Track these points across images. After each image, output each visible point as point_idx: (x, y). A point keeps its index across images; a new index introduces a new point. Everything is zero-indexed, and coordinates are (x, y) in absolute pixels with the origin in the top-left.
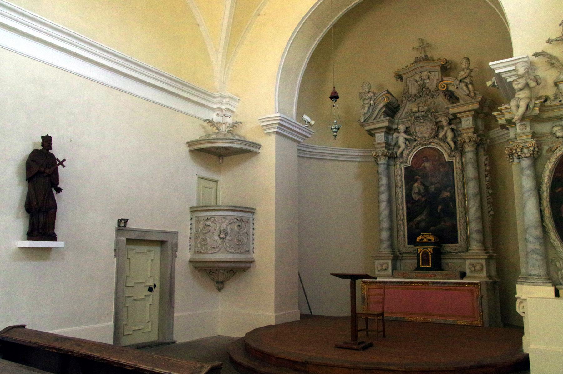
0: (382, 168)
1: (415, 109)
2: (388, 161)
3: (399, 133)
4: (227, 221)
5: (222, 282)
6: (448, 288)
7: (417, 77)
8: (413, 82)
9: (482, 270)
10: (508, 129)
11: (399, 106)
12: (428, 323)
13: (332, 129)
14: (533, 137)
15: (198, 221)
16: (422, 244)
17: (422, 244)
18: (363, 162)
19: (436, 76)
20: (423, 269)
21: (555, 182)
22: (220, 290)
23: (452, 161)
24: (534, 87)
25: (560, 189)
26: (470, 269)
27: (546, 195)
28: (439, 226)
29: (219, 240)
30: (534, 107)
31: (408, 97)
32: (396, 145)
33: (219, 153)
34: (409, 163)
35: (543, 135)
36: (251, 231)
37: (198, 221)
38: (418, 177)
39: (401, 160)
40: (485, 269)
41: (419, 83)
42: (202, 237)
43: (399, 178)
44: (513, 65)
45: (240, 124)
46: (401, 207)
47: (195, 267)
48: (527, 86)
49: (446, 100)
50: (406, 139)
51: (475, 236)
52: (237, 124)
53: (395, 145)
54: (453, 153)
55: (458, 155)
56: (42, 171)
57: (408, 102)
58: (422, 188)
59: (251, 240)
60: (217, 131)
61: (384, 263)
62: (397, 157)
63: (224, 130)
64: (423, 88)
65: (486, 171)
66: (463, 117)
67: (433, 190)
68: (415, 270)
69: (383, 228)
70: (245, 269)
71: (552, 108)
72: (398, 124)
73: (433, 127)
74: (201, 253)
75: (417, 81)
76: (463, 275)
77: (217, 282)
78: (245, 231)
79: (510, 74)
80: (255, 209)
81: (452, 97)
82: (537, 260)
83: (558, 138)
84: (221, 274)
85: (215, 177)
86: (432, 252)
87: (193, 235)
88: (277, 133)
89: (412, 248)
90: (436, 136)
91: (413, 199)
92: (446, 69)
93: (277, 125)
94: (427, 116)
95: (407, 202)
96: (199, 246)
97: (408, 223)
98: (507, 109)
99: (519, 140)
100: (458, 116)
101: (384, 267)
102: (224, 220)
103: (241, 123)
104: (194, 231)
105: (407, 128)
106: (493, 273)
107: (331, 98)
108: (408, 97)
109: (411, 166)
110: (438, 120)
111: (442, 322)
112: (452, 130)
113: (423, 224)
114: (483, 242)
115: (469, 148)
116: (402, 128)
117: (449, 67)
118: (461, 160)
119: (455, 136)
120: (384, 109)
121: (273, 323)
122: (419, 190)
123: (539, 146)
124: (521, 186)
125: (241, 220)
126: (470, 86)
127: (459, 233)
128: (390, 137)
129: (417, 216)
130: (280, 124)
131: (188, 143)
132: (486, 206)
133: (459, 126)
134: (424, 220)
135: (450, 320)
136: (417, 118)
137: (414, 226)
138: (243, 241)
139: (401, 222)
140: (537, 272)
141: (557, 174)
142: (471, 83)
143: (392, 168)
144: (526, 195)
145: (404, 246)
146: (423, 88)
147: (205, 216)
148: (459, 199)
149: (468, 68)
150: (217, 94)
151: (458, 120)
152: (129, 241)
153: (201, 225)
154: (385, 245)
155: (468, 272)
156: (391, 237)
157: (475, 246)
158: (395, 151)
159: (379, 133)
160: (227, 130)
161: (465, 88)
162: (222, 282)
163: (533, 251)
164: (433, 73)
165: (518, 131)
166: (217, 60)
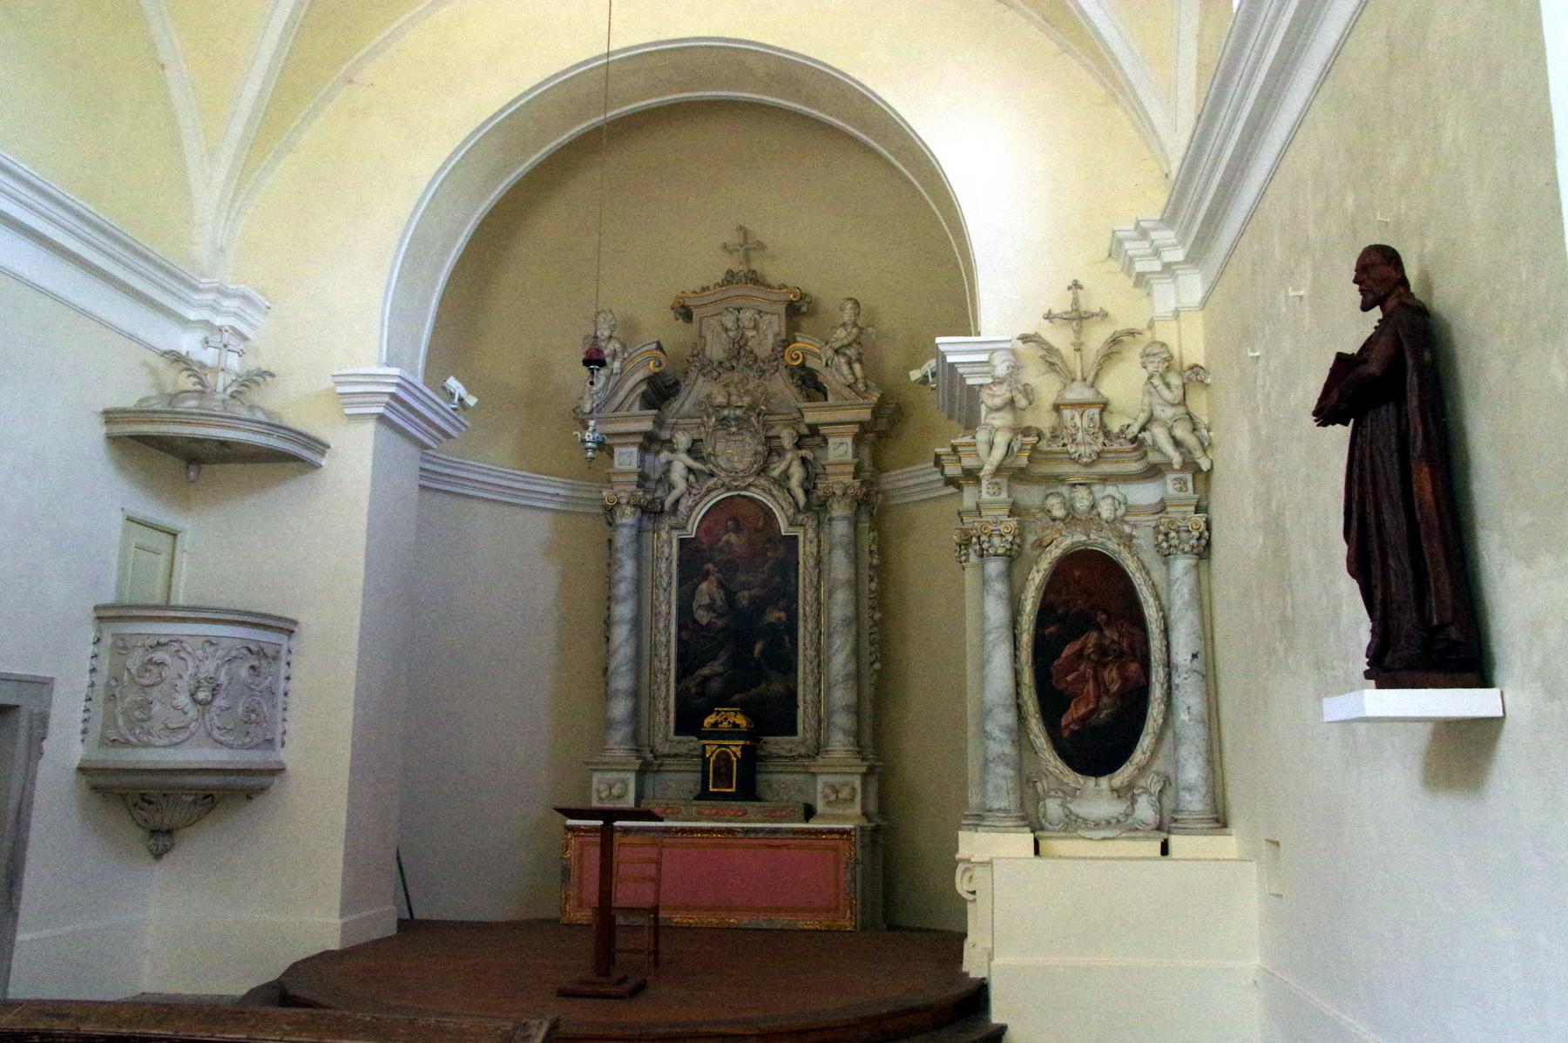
0: (624, 537)
1: (720, 399)
2: (640, 521)
3: (673, 451)
5: (169, 832)
6: (779, 842)
7: (729, 321)
9: (852, 800)
10: (959, 487)
11: (677, 383)
12: (730, 929)
13: (584, 441)
14: (1011, 514)
15: (125, 648)
16: (716, 733)
18: (558, 511)
19: (774, 325)
20: (715, 796)
21: (1045, 612)
22: (158, 856)
23: (796, 537)
24: (1024, 410)
25: (1052, 629)
27: (1026, 639)
30: (1020, 450)
31: (703, 367)
32: (665, 480)
33: (190, 453)
34: (691, 531)
35: (1027, 509)
36: (282, 683)
37: (122, 647)
38: (710, 566)
39: (673, 521)
40: (858, 798)
41: (731, 334)
42: (133, 696)
43: (663, 566)
44: (985, 351)
46: (663, 639)
47: (95, 788)
48: (1012, 402)
49: (795, 390)
50: (690, 470)
52: (253, 380)
53: (659, 481)
54: (800, 517)
55: (811, 524)
57: (701, 379)
58: (719, 595)
59: (280, 707)
60: (198, 387)
61: (617, 780)
62: (662, 511)
63: (220, 388)
64: (739, 348)
65: (871, 567)
66: (834, 435)
67: (745, 603)
68: (697, 798)
69: (617, 691)
70: (250, 794)
71: (1051, 456)
72: (674, 428)
73: (760, 448)
74: (127, 743)
75: (727, 330)
76: (809, 812)
78: (267, 683)
79: (976, 369)
80: (295, 623)
81: (810, 384)
82: (1005, 777)
83: (1054, 520)
84: (157, 808)
85: (168, 519)
87: (100, 688)
88: (381, 418)
89: (691, 743)
90: (763, 470)
91: (695, 621)
92: (798, 310)
93: (387, 399)
94: (747, 420)
95: (680, 628)
96: (120, 722)
97: (678, 681)
98: (969, 445)
100: (823, 430)
101: (615, 791)
102: (210, 650)
103: (272, 375)
104: (101, 679)
105: (694, 441)
106: (873, 807)
107: (586, 363)
108: (703, 367)
110: (770, 433)
112: (804, 460)
113: (715, 685)
114: (857, 736)
115: (839, 510)
116: (683, 440)
117: (804, 309)
118: (818, 536)
119: (807, 478)
120: (644, 387)
121: (334, 943)
122: (712, 599)
123: (1020, 533)
124: (982, 616)
125: (261, 653)
126: (857, 367)
127: (800, 712)
128: (649, 458)
129: (702, 666)
130: (393, 396)
131: (106, 413)
132: (866, 647)
133: (819, 453)
134: (720, 675)
135: (782, 921)
136: (723, 421)
137: (693, 690)
138: (258, 714)
139: (661, 677)
140: (1004, 804)
141: (1051, 597)
142: (859, 360)
143: (647, 537)
144: (991, 637)
146: (739, 348)
149: (855, 324)
150: (204, 282)
151: (818, 440)
153: (134, 661)
154: (619, 735)
155: (820, 807)
156: (636, 713)
157: (839, 744)
158: (659, 494)
159: (626, 444)
160: (229, 391)
161: (845, 369)
162: (169, 832)
163: (1001, 758)
165: (985, 496)
166: (208, 183)
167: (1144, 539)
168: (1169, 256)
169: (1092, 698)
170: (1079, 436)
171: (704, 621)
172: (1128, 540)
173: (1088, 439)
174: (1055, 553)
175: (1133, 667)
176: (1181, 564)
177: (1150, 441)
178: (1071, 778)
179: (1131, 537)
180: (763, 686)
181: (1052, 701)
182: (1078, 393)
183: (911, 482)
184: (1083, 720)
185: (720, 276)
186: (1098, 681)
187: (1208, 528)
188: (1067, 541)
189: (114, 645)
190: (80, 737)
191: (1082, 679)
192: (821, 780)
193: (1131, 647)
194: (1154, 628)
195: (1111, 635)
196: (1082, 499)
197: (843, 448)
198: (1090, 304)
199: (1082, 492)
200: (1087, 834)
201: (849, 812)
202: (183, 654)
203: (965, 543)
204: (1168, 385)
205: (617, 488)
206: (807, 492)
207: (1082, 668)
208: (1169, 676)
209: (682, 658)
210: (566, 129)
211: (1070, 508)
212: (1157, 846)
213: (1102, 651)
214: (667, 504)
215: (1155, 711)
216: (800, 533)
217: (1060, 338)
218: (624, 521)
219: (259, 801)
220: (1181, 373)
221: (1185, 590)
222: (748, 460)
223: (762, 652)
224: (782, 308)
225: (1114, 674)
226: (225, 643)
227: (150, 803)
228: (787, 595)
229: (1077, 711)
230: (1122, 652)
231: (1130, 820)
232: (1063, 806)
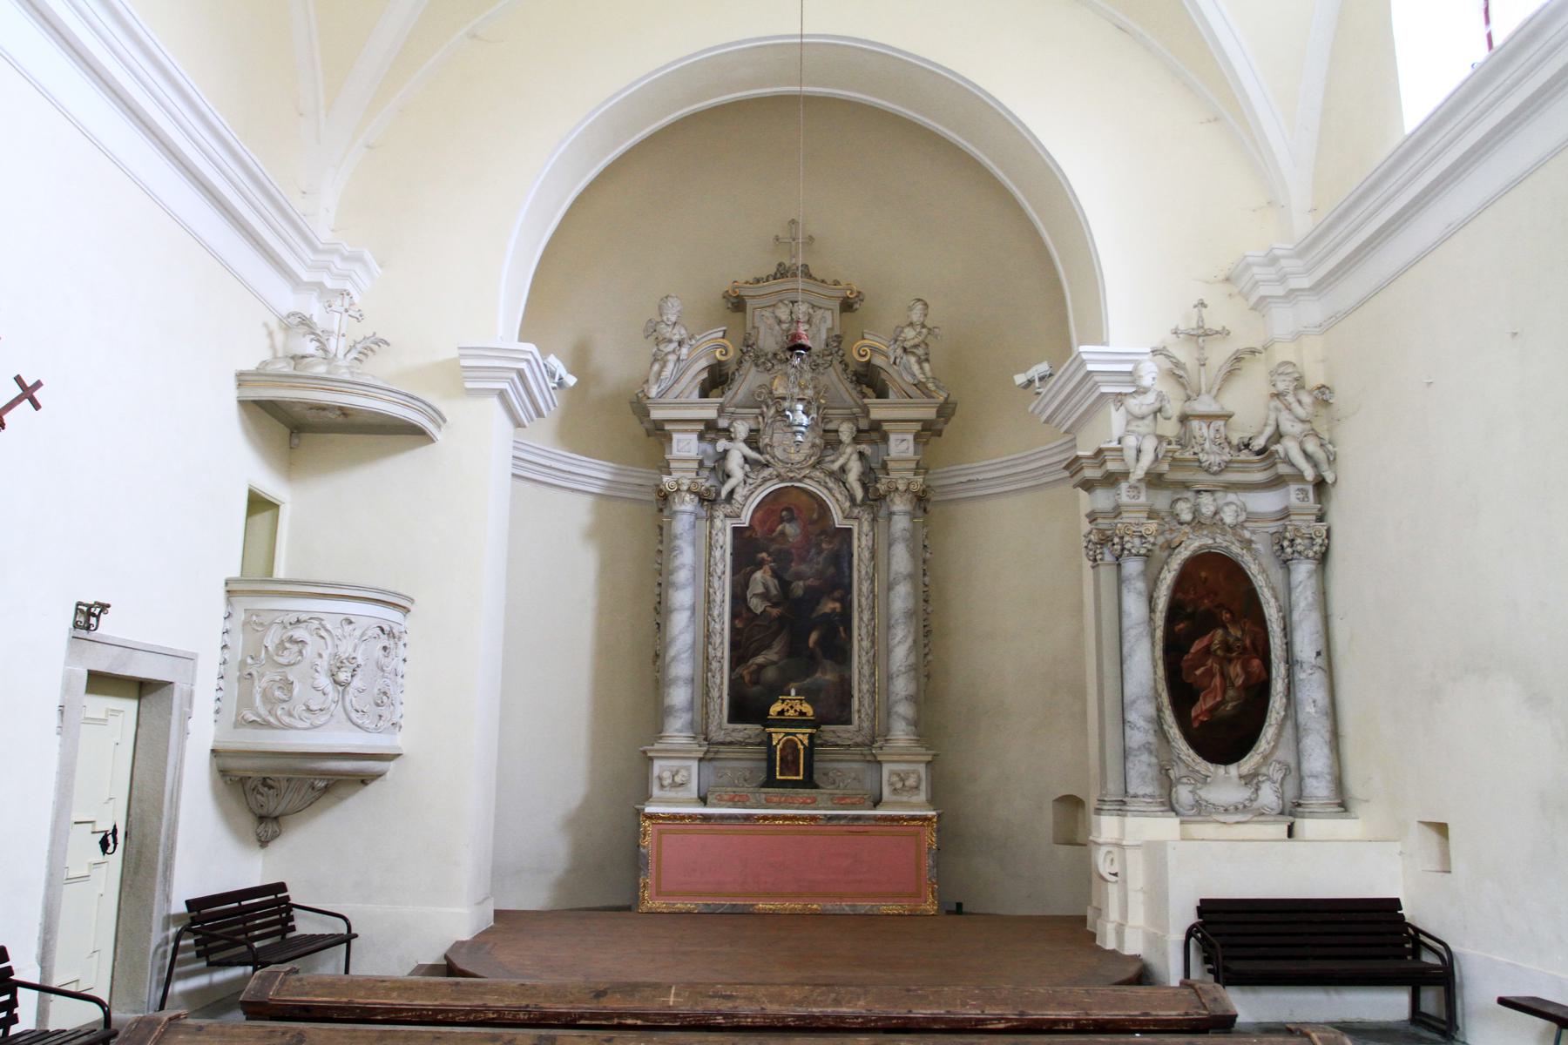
3: (731, 439)
4: (358, 633)
5: (276, 818)
7: (783, 313)
8: (771, 321)
9: (917, 788)
16: (782, 721)
17: (782, 721)
21: (1175, 611)
22: (264, 843)
23: (850, 530)
26: (891, 784)
29: (330, 688)
31: (757, 357)
34: (745, 520)
37: (255, 625)
39: (728, 509)
40: (923, 786)
42: (272, 675)
45: (384, 347)
46: (718, 627)
51: (904, 709)
54: (856, 511)
55: (866, 517)
57: (754, 369)
58: (773, 584)
66: (896, 432)
70: (364, 780)
73: (817, 441)
74: (266, 725)
75: (780, 322)
77: (262, 819)
80: (412, 600)
86: (806, 742)
91: (749, 609)
95: (734, 616)
97: (732, 669)
99: (1127, 517)
100: (886, 427)
102: (348, 628)
104: (237, 653)
108: (757, 357)
109: (751, 527)
110: (831, 426)
111: (848, 910)
112: (861, 455)
113: (770, 674)
115: (900, 505)
116: (741, 429)
134: (773, 663)
137: (747, 678)
141: (1179, 595)
145: (720, 727)
148: (861, 619)
151: (874, 435)
152: (100, 682)
153: (271, 640)
157: (901, 733)
161: (916, 368)
164: (820, 312)
168: (1295, 283)
169: (1219, 692)
170: (1207, 446)
172: (1248, 544)
173: (1215, 448)
174: (1184, 554)
175: (1256, 663)
176: (1303, 571)
177: (1282, 454)
178: (1204, 766)
179: (1250, 542)
180: (818, 675)
182: (1204, 405)
183: (964, 479)
185: (773, 270)
186: (1224, 676)
187: (1328, 537)
188: (1193, 544)
189: (246, 624)
190: (213, 717)
191: (1209, 673)
192: (886, 769)
193: (1253, 643)
194: (1275, 627)
195: (1235, 632)
196: (1207, 504)
197: (904, 446)
198: (1213, 322)
199: (1206, 499)
200: (1222, 818)
201: (915, 799)
203: (1105, 541)
204: (1299, 402)
205: (676, 475)
206: (865, 487)
207: (1209, 662)
208: (1290, 675)
209: (734, 645)
210: (667, 114)
211: (1196, 511)
212: (1285, 828)
213: (1227, 647)
214: (724, 493)
215: (1277, 703)
216: (855, 526)
217: (1183, 354)
218: (683, 508)
219: (373, 787)
220: (1310, 392)
221: (1309, 594)
222: (805, 450)
223: (817, 643)
224: (836, 305)
225: (1239, 669)
226: (360, 623)
227: (271, 787)
228: (839, 584)
230: (1245, 648)
231: (1255, 805)
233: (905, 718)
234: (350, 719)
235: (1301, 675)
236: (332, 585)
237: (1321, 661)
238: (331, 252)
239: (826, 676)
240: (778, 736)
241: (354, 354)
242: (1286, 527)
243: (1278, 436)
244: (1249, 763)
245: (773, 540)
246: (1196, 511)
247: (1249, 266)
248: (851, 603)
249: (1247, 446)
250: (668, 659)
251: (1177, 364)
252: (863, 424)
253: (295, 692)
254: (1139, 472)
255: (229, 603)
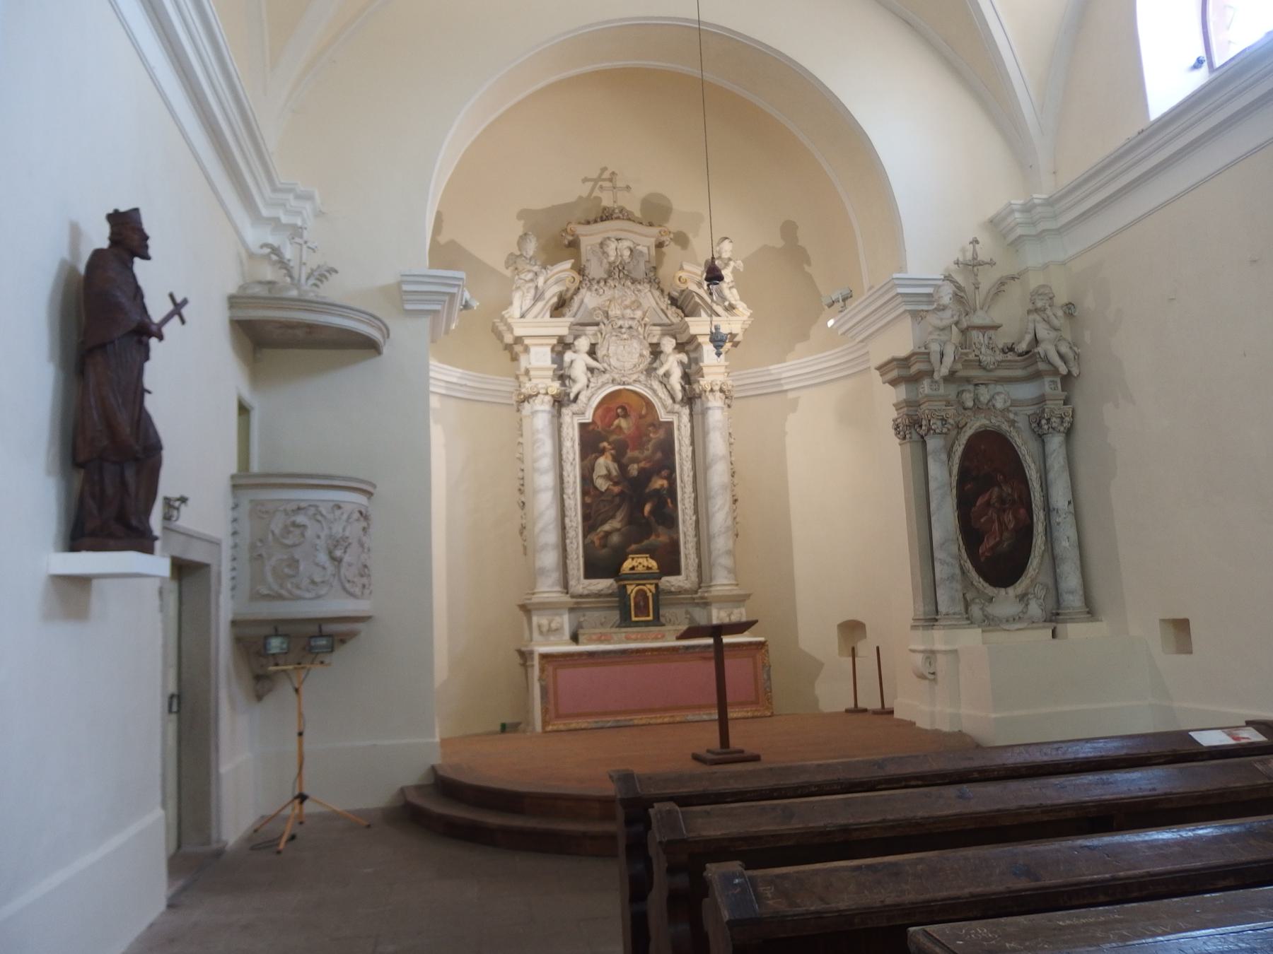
4: (345, 517)
20: (637, 624)
22: (259, 697)
23: (671, 423)
28: (646, 542)
34: (588, 418)
37: (261, 512)
39: (574, 407)
50: (591, 370)
51: (725, 561)
52: (322, 275)
55: (686, 411)
56: (103, 318)
70: (343, 639)
74: (280, 597)
80: (374, 486)
83: (965, 409)
91: (596, 488)
95: (585, 493)
96: (270, 578)
97: (585, 536)
100: (527, 341)
102: (338, 512)
109: (593, 422)
113: (615, 539)
122: (609, 471)
129: (603, 522)
137: (597, 543)
147: (289, 501)
153: (277, 525)
167: (1022, 423)
171: (603, 489)
172: (1012, 423)
173: (989, 352)
174: (969, 432)
175: (1022, 511)
176: (1055, 442)
178: (990, 590)
180: (653, 537)
181: (970, 533)
182: (979, 319)
184: (992, 548)
186: (1000, 523)
188: (976, 424)
195: (1007, 489)
196: (984, 394)
199: (982, 390)
200: (1007, 627)
202: (319, 518)
205: (534, 381)
209: (586, 517)
211: (976, 399)
213: (1002, 500)
222: (635, 359)
223: (651, 512)
229: (988, 543)
232: (982, 609)
233: (726, 568)
234: (344, 589)
235: (1056, 519)
236: (344, 478)
237: (1072, 508)
238: (290, 191)
239: (661, 537)
240: (632, 589)
241: (312, 281)
242: (1043, 411)
243: (1036, 341)
244: (1021, 585)
245: (613, 432)
246: (976, 399)
247: (1012, 211)
248: (675, 480)
249: (1011, 349)
250: (537, 530)
251: (959, 287)
252: (683, 338)
253: (301, 568)
254: (944, 371)
255: (234, 495)
